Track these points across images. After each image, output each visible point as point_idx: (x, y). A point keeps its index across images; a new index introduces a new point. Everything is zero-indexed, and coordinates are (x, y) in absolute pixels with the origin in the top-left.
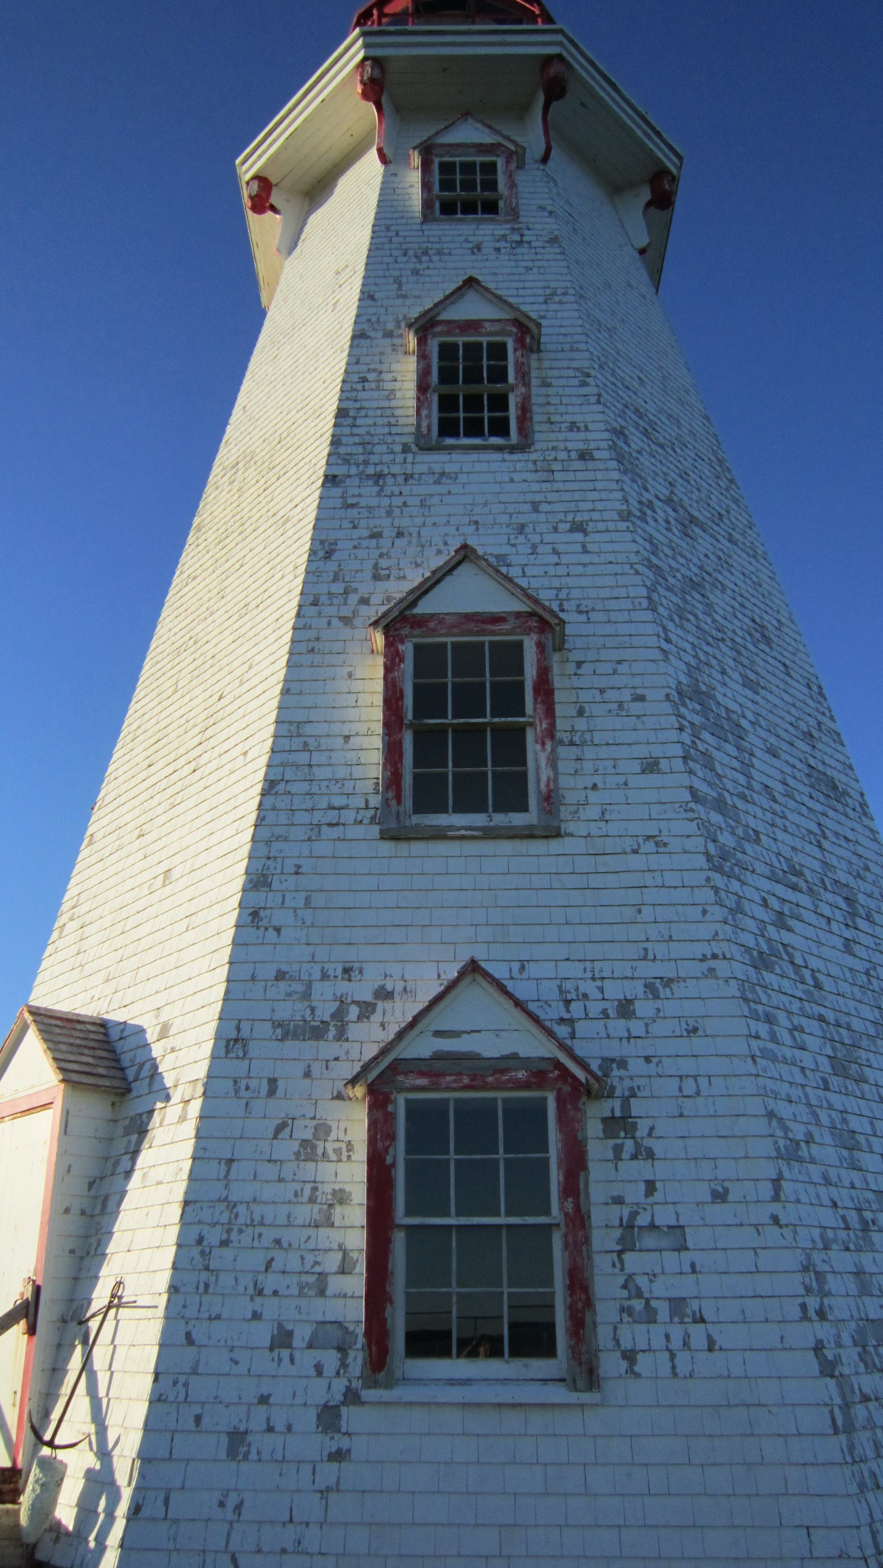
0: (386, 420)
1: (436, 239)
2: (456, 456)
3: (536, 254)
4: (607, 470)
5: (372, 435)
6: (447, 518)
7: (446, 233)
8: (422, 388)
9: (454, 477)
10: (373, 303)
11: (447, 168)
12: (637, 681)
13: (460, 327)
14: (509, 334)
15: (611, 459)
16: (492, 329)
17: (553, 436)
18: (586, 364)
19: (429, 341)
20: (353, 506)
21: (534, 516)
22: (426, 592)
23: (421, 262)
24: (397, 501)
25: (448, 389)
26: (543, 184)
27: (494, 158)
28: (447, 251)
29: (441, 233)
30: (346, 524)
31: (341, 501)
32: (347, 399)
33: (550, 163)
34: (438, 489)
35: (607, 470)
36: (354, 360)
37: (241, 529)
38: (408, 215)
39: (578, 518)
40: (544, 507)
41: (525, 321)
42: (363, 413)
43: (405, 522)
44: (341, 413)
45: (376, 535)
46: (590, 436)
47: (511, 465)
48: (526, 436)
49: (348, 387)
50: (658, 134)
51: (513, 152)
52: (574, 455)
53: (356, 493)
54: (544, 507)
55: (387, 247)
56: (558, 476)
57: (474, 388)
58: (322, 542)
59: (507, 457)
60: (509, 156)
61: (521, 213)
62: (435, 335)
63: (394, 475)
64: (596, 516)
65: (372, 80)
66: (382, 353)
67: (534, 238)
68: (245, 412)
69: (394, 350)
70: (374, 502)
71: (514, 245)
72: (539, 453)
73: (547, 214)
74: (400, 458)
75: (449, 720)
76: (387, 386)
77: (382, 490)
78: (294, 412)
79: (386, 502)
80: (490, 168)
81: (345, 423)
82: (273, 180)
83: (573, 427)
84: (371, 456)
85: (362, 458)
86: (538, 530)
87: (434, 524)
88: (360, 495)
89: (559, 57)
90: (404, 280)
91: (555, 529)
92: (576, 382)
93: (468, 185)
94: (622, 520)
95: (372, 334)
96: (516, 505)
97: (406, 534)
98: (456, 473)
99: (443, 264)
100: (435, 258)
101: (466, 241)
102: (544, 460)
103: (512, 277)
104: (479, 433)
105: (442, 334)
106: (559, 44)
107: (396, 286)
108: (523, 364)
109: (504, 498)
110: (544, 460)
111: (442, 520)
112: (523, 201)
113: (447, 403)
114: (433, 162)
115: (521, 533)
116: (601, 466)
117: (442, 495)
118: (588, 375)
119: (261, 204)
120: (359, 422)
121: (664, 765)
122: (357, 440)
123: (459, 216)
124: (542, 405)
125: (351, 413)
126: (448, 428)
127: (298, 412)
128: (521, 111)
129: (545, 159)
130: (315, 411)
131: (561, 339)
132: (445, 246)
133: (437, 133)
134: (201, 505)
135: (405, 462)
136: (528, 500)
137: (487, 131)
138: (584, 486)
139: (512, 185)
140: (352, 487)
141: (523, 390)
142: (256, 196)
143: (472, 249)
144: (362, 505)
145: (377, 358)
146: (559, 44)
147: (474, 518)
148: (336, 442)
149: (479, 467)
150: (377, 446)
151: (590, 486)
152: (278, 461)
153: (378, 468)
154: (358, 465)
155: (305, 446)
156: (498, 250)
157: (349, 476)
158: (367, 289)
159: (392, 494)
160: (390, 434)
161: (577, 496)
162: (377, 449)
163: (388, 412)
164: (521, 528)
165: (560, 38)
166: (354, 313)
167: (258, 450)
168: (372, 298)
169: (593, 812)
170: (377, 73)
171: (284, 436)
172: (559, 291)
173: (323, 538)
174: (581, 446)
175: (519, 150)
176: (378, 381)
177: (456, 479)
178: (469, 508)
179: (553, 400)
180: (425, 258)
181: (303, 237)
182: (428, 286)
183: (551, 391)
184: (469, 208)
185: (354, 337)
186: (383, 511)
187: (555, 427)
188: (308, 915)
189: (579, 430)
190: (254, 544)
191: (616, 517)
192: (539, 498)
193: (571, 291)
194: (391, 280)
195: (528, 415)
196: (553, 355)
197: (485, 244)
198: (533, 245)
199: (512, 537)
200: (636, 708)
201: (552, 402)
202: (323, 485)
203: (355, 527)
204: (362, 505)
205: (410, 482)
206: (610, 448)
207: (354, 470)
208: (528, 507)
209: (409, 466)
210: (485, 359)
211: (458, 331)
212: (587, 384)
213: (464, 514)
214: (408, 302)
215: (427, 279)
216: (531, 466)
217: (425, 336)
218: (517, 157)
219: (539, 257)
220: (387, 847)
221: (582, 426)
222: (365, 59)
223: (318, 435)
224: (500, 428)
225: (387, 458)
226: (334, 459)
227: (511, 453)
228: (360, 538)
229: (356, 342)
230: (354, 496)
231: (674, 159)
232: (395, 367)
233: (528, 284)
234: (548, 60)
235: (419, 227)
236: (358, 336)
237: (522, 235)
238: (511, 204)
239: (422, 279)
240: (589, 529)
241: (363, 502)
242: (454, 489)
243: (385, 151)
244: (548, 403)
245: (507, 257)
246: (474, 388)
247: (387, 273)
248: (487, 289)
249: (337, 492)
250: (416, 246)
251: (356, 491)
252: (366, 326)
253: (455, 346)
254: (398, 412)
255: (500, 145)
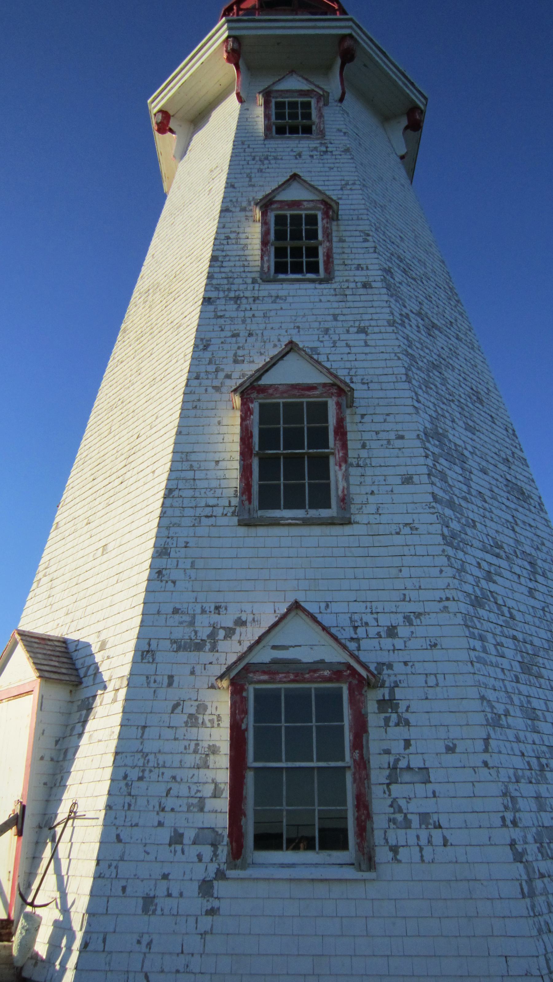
0: (241, 263)
1: (273, 150)
2: (285, 286)
3: (336, 159)
4: (380, 294)
5: (233, 273)
6: (280, 325)
7: (279, 146)
8: (265, 243)
9: (284, 299)
10: (234, 190)
11: (280, 105)
12: (399, 427)
13: (288, 205)
14: (319, 209)
15: (383, 287)
16: (308, 206)
17: (346, 273)
18: (367, 228)
19: (269, 214)
20: (221, 317)
21: (334, 323)
22: (267, 371)
23: (263, 164)
24: (249, 314)
25: (281, 244)
26: (340, 115)
27: (309, 99)
28: (280, 157)
29: (276, 146)
30: (217, 328)
31: (213, 314)
32: (218, 250)
33: (345, 102)
34: (274, 306)
35: (380, 294)
36: (222, 225)
37: (151, 331)
38: (256, 135)
39: (362, 325)
40: (340, 318)
41: (329, 201)
42: (227, 259)
43: (254, 327)
44: (214, 259)
45: (235, 335)
46: (370, 273)
47: (320, 291)
48: (329, 273)
49: (218, 242)
50: (412, 84)
51: (321, 95)
52: (359, 285)
53: (223, 309)
54: (340, 318)
55: (242, 154)
56: (349, 298)
57: (297, 243)
58: (202, 340)
59: (318, 286)
60: (319, 97)
61: (326, 133)
62: (272, 210)
63: (247, 298)
64: (373, 323)
65: (233, 50)
66: (239, 221)
67: (335, 149)
68: (153, 258)
69: (246, 219)
70: (234, 314)
71: (322, 153)
72: (338, 284)
73: (342, 134)
74: (250, 287)
75: (281, 451)
76: (242, 242)
77: (239, 307)
78: (184, 258)
79: (241, 314)
80: (307, 105)
81: (216, 265)
82: (171, 113)
83: (359, 267)
84: (232, 286)
85: (226, 287)
86: (337, 332)
87: (272, 328)
88: (225, 310)
89: (350, 36)
90: (253, 175)
91: (348, 332)
92: (361, 239)
93: (293, 116)
94: (390, 326)
95: (233, 209)
96: (323, 317)
97: (254, 335)
98: (286, 297)
99: (277, 166)
100: (272, 162)
101: (292, 151)
102: (341, 288)
103: (320, 174)
104: (300, 271)
105: (277, 209)
106: (350, 27)
107: (248, 179)
108: (327, 228)
109: (315, 312)
110: (341, 288)
111: (277, 326)
112: (328, 126)
113: (280, 252)
114: (271, 101)
115: (326, 334)
116: (376, 292)
117: (277, 310)
118: (368, 235)
119: (163, 128)
120: (225, 264)
121: (416, 479)
122: (224, 275)
123: (287, 135)
124: (339, 254)
125: (220, 259)
126: (280, 268)
127: (187, 258)
128: (326, 70)
129: (341, 100)
130: (197, 258)
131: (352, 212)
132: (279, 154)
133: (274, 84)
134: (126, 316)
135: (253, 289)
136: (331, 313)
137: (305, 82)
138: (366, 304)
139: (321, 116)
140: (221, 305)
141: (328, 244)
142: (161, 123)
143: (295, 156)
144: (226, 316)
145: (236, 224)
146: (350, 27)
147: (297, 325)
148: (210, 277)
149: (300, 292)
150: (236, 280)
151: (370, 304)
152: (174, 289)
153: (237, 293)
154: (224, 291)
155: (191, 279)
156: (312, 156)
157: (219, 298)
158: (230, 181)
159: (246, 310)
160: (244, 272)
161: (361, 311)
162: (236, 281)
163: (243, 258)
164: (327, 331)
165: (350, 24)
166: (222, 196)
167: (162, 282)
168: (233, 186)
169: (371, 509)
170: (236, 46)
171: (178, 273)
172: (350, 183)
173: (203, 337)
174: (364, 279)
175: (325, 94)
176: (237, 239)
177: (286, 300)
178: (294, 318)
179: (346, 251)
180: (266, 162)
181: (190, 148)
182: (268, 179)
183: (345, 245)
184: (294, 130)
185: (221, 211)
186: (240, 320)
187: (348, 268)
188: (193, 573)
189: (362, 269)
190: (159, 341)
191: (386, 324)
192: (337, 312)
193: (358, 182)
194: (245, 175)
195: (331, 260)
196: (346, 223)
197: (304, 153)
198: (334, 153)
199: (321, 336)
200: (398, 443)
201: (346, 252)
202: (202, 304)
203: (222, 330)
204: (226, 316)
205: (257, 302)
206: (382, 280)
207: (221, 295)
208: (330, 318)
209: (256, 292)
210: (304, 225)
211: (287, 207)
212: (368, 241)
213: (291, 322)
214: (256, 189)
215: (268, 175)
216: (332, 292)
217: (266, 211)
218: (324, 98)
219: (338, 161)
220: (242, 531)
221: (364, 267)
222: (228, 37)
223: (199, 272)
224: (313, 268)
225: (242, 287)
226: (209, 288)
227: (320, 284)
228: (225, 337)
229: (223, 214)
230: (221, 310)
231: (422, 99)
232: (247, 230)
233: (331, 178)
234: (343, 37)
235: (262, 142)
236: (224, 211)
237: (327, 147)
238: (320, 127)
239: (264, 175)
240: (369, 332)
241: (227, 314)
242: (284, 306)
243: (241, 94)
244: (343, 253)
245: (317, 161)
246: (297, 243)
247: (242, 171)
248: (305, 181)
249: (211, 308)
250: (261, 154)
251: (223, 308)
252: (229, 204)
253: (285, 216)
254: (249, 258)
255: (313, 91)
